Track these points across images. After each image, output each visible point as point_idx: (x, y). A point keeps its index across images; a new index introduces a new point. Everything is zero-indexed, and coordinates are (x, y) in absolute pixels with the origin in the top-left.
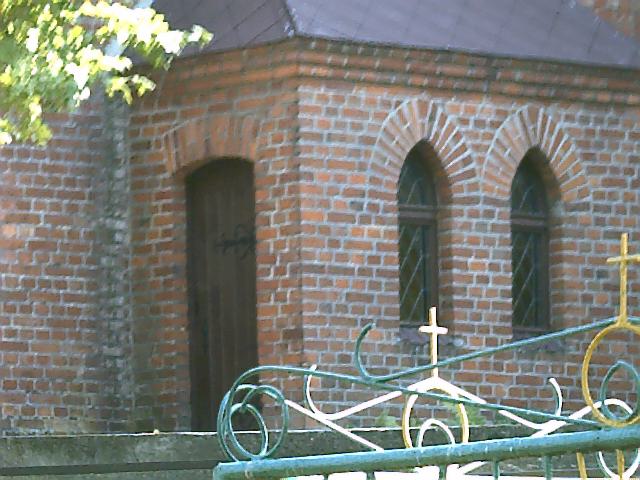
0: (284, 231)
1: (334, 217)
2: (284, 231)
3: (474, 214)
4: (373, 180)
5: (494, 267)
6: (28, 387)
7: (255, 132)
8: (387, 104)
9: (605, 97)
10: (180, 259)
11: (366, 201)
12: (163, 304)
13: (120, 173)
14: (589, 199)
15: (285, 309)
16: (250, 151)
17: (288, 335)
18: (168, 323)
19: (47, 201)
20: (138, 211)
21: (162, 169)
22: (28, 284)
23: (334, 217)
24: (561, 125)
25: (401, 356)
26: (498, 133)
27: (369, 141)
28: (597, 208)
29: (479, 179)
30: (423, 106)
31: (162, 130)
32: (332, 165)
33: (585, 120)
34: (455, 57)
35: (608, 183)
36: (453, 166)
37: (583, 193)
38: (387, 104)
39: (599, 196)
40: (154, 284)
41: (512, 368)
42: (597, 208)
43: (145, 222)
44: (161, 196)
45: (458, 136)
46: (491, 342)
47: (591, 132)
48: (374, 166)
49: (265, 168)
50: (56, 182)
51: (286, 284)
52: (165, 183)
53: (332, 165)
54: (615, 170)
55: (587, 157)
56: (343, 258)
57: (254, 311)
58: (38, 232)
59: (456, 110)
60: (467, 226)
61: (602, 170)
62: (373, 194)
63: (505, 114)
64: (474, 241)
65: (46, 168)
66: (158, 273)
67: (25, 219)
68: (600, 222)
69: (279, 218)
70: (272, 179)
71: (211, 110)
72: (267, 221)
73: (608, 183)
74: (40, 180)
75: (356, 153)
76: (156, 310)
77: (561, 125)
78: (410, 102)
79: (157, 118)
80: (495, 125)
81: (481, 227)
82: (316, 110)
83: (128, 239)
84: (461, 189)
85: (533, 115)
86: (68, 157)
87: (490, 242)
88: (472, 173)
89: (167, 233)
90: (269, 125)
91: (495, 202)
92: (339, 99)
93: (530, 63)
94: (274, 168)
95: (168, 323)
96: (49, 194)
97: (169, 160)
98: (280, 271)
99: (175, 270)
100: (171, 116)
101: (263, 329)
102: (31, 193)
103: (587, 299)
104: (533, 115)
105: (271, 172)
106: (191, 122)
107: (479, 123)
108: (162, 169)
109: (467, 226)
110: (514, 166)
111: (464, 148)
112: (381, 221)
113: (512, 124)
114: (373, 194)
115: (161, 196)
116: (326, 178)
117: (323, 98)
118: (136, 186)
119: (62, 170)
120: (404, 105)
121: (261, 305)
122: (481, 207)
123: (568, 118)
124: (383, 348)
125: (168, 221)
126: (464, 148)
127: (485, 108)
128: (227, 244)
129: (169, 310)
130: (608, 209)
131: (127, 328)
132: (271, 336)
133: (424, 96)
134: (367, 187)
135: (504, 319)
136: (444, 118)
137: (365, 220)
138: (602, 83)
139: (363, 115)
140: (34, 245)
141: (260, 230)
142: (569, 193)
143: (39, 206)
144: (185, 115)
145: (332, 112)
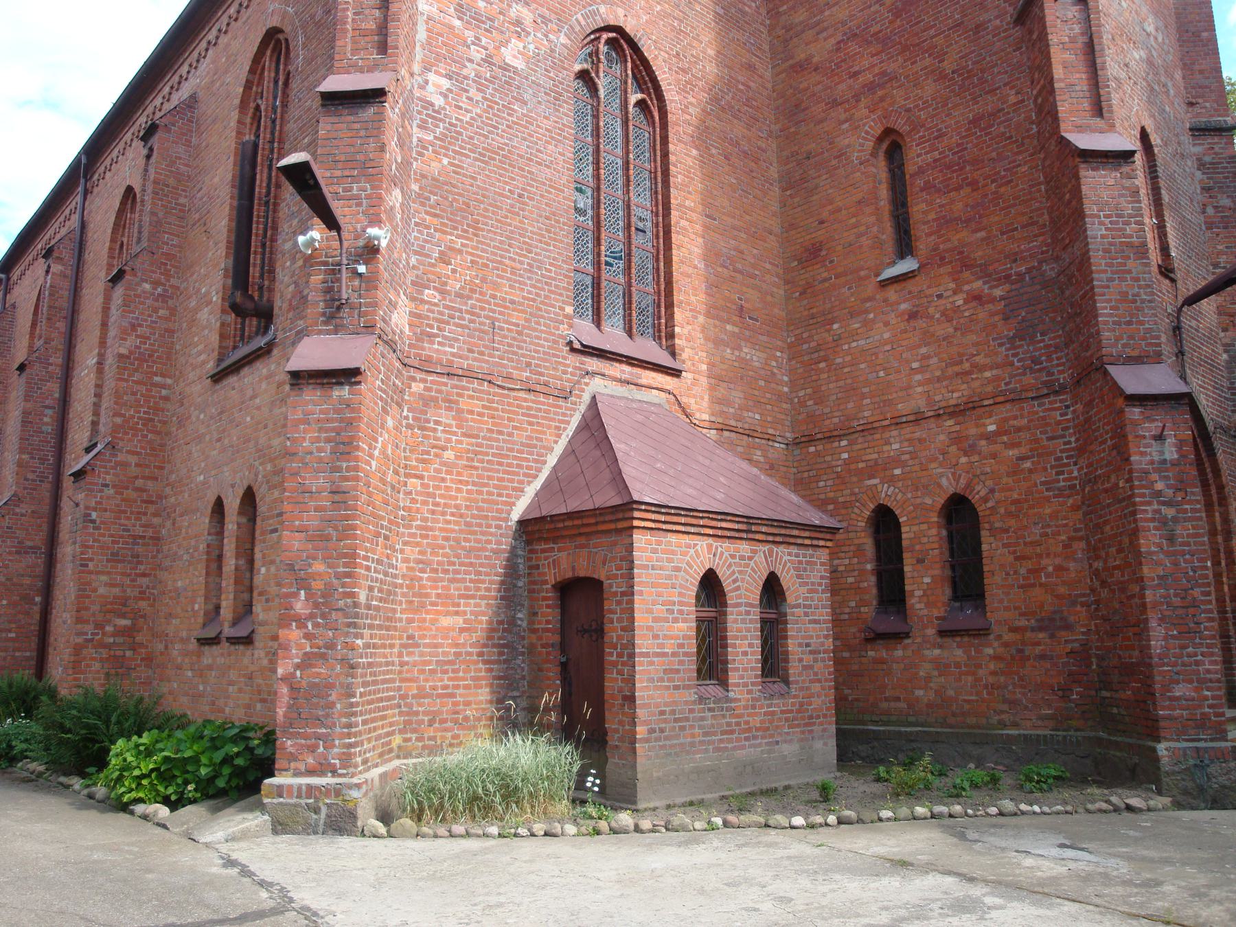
0: (623, 629)
1: (656, 620)
2: (623, 629)
3: (740, 614)
4: (680, 594)
5: (751, 645)
6: (456, 721)
7: (604, 564)
8: (689, 546)
9: (807, 542)
10: (556, 638)
11: (676, 608)
12: (546, 666)
13: (520, 584)
14: (800, 601)
15: (623, 680)
16: (601, 574)
17: (625, 698)
18: (549, 679)
19: (472, 601)
20: (532, 607)
21: (546, 582)
22: (457, 654)
23: (656, 620)
24: (786, 558)
25: (696, 707)
26: (752, 563)
27: (678, 569)
28: (805, 607)
29: (743, 591)
30: (710, 546)
31: (546, 558)
32: (654, 585)
33: (797, 555)
34: (246, 596)
35: (810, 591)
36: (727, 585)
37: (797, 598)
38: (689, 546)
39: (806, 599)
40: (540, 653)
41: (761, 707)
42: (805, 607)
43: (535, 614)
44: (545, 599)
45: (730, 565)
46: (749, 692)
47: (800, 562)
48: (681, 586)
49: (611, 586)
50: (478, 589)
51: (624, 664)
52: (547, 591)
53: (654, 585)
54: (813, 584)
55: (799, 577)
56: (661, 646)
57: (602, 679)
58: (465, 621)
59: (728, 549)
60: (735, 621)
61: (807, 584)
62: (681, 603)
63: (754, 552)
64: (739, 630)
65: (471, 581)
66: (543, 646)
67: (457, 613)
68: (806, 614)
69: (620, 620)
70: (615, 594)
71: (576, 547)
72: (612, 622)
73: (810, 591)
74: (467, 589)
75: (669, 577)
76: (540, 670)
77: (786, 558)
78: (702, 544)
79: (543, 551)
80: (750, 558)
81: (743, 621)
82: (798, 606)
83: (525, 624)
84: (731, 598)
85: (771, 551)
86: (487, 574)
87: (748, 630)
88: (738, 588)
89: (548, 622)
90: (613, 559)
91: (752, 605)
92: (659, 543)
93: (770, 522)
94: (614, 587)
95: (549, 679)
96: (473, 597)
97: (551, 577)
98: (620, 655)
99: (552, 645)
100: (552, 549)
101: (608, 692)
102: (461, 596)
103: (801, 660)
104: (771, 551)
105: (614, 589)
106: (563, 554)
107: (742, 558)
108: (546, 582)
109: (735, 621)
110: (761, 583)
111: (733, 572)
112: (685, 621)
113: (760, 557)
114: (681, 603)
115: (545, 599)
116: (650, 594)
117: (649, 542)
118: (531, 591)
119: (483, 582)
120: (698, 548)
121: (607, 676)
122: (743, 609)
123: (790, 554)
124: (686, 703)
125: (549, 615)
126: (733, 572)
127: (744, 548)
128: (586, 631)
129: (548, 670)
130: (810, 606)
131: (523, 678)
132: (613, 697)
133: (710, 540)
134: (676, 599)
135: (756, 676)
136: (722, 554)
137: (676, 620)
138: (807, 534)
139: (674, 553)
140: (462, 630)
141: (607, 626)
142: (790, 599)
143: (467, 605)
144: (560, 550)
145: (655, 551)
